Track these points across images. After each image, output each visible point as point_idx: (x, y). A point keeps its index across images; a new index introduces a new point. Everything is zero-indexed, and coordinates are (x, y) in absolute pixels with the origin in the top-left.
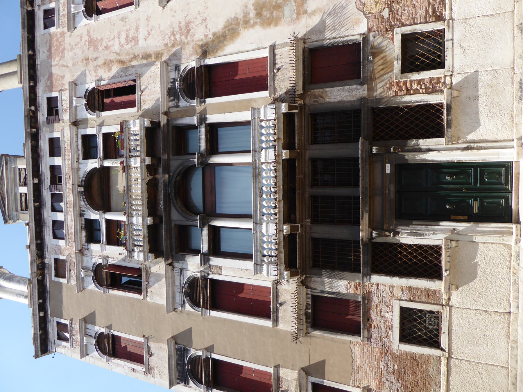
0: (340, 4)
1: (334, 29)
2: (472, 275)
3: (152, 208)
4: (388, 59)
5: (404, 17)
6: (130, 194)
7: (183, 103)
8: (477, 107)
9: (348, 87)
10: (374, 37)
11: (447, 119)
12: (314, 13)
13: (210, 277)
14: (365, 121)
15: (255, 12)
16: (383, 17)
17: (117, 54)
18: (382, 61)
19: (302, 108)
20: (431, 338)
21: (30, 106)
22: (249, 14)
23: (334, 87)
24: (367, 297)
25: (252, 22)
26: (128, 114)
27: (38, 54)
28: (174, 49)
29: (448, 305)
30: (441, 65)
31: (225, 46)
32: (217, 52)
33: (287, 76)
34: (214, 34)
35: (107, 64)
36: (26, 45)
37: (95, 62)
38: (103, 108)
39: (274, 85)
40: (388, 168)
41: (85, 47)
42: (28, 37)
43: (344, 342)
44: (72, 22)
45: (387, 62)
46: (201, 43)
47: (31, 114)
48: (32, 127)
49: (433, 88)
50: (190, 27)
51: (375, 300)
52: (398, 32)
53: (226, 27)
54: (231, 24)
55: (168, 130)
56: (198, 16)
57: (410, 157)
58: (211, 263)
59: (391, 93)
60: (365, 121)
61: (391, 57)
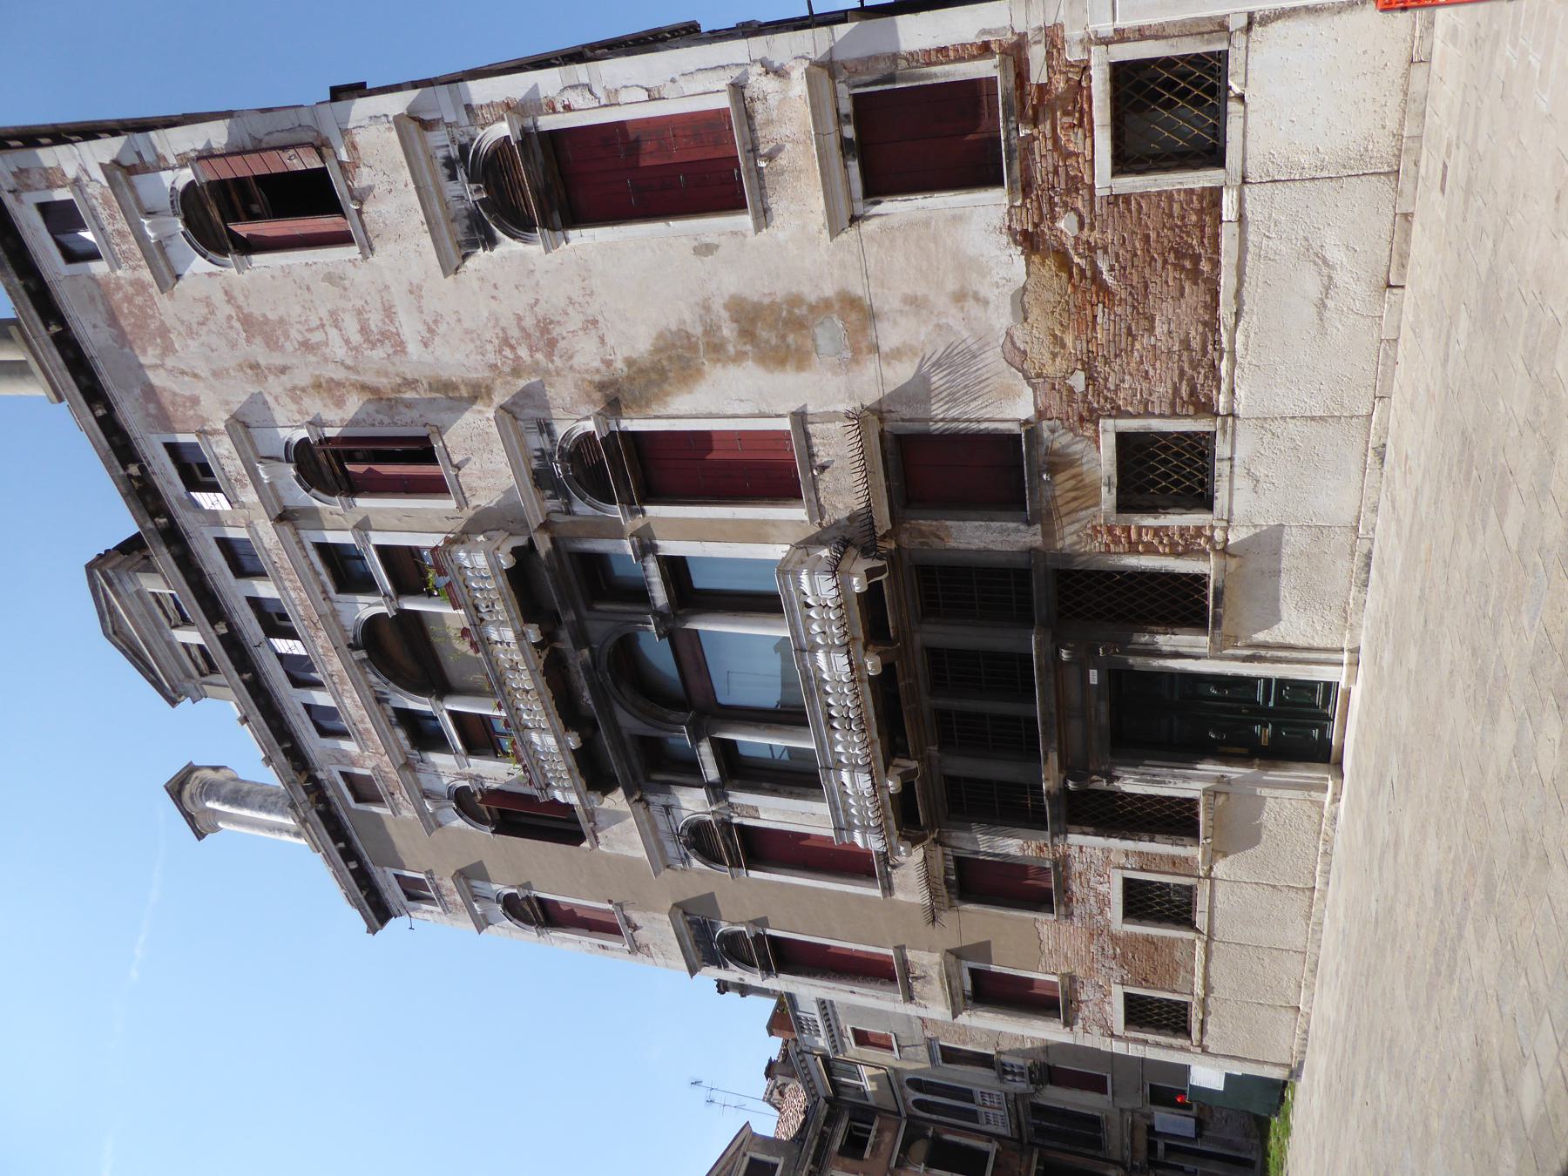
0: (963, 346)
1: (953, 399)
2: (1251, 837)
3: (568, 712)
4: (1087, 481)
5: (1122, 395)
6: (506, 690)
7: (581, 508)
8: (1277, 590)
9: (998, 524)
10: (1053, 431)
11: (1215, 614)
12: (897, 354)
13: (736, 820)
14: (1042, 596)
15: (735, 325)
16: (1071, 390)
17: (348, 368)
18: (1072, 482)
19: (894, 559)
20: (1190, 489)
21: (125, 468)
22: (719, 328)
23: (964, 520)
24: (1062, 864)
25: (731, 349)
26: (436, 511)
27: (81, 332)
28: (522, 383)
29: (1208, 876)
30: (1205, 502)
31: (667, 394)
32: (648, 404)
33: (846, 484)
34: (630, 362)
35: (328, 388)
36: (33, 313)
37: (284, 378)
38: (353, 487)
39: (818, 500)
40: (1094, 677)
41: (233, 334)
42: (26, 287)
43: (1025, 920)
44: (161, 263)
45: (1085, 486)
46: (597, 378)
47: (136, 484)
48: (153, 516)
49: (1187, 545)
50: (554, 334)
51: (1077, 867)
52: (1109, 430)
53: (658, 350)
54: (674, 345)
55: (561, 562)
56: (570, 309)
57: (1137, 662)
58: (731, 800)
59: (1096, 546)
60: (1042, 596)
61: (1093, 477)
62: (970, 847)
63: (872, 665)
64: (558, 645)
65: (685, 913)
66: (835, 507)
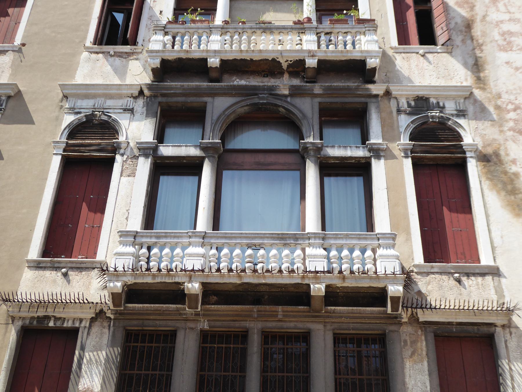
3: (233, 66)
13: (118, 158)
23: (430, 374)
28: (491, 109)
31: (498, 192)
39: (433, 273)
46: (502, 153)
58: (141, 159)
62: (90, 343)
63: (194, 287)
64: (286, 76)
65: (9, 97)
66: (429, 284)
